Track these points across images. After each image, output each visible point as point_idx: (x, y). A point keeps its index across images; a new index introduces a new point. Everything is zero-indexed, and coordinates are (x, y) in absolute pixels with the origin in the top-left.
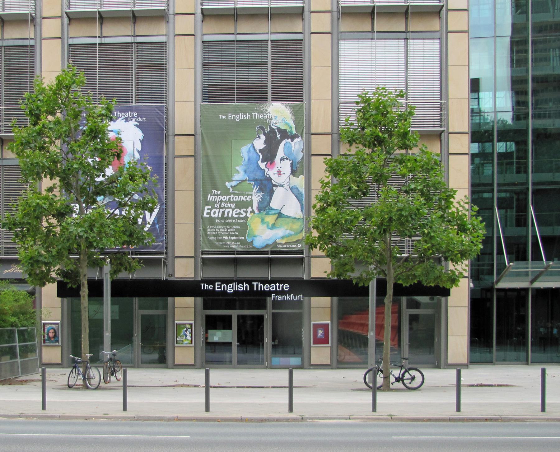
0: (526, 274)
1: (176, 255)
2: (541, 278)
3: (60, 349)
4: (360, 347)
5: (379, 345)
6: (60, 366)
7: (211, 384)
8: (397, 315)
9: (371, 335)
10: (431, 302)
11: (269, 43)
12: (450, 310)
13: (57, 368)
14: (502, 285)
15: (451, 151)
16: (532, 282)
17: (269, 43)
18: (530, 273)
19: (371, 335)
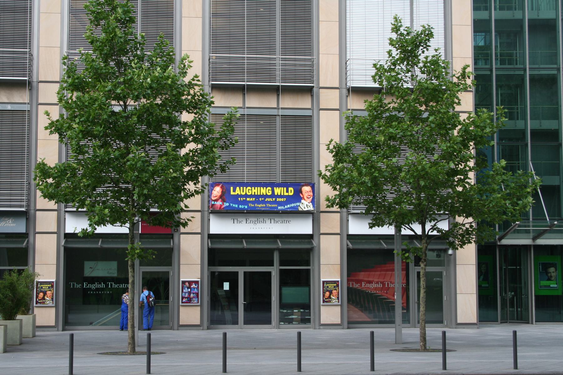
0: (528, 232)
1: (37, 208)
2: (546, 235)
3: (199, 308)
4: (379, 311)
5: (406, 307)
6: (341, 327)
7: (441, 354)
8: (405, 272)
9: (398, 297)
10: (437, 259)
11: (278, 119)
12: (339, 262)
13: (334, 329)
14: (505, 242)
15: (40, 101)
16: (534, 239)
17: (278, 119)
18: (531, 231)
19: (398, 297)
